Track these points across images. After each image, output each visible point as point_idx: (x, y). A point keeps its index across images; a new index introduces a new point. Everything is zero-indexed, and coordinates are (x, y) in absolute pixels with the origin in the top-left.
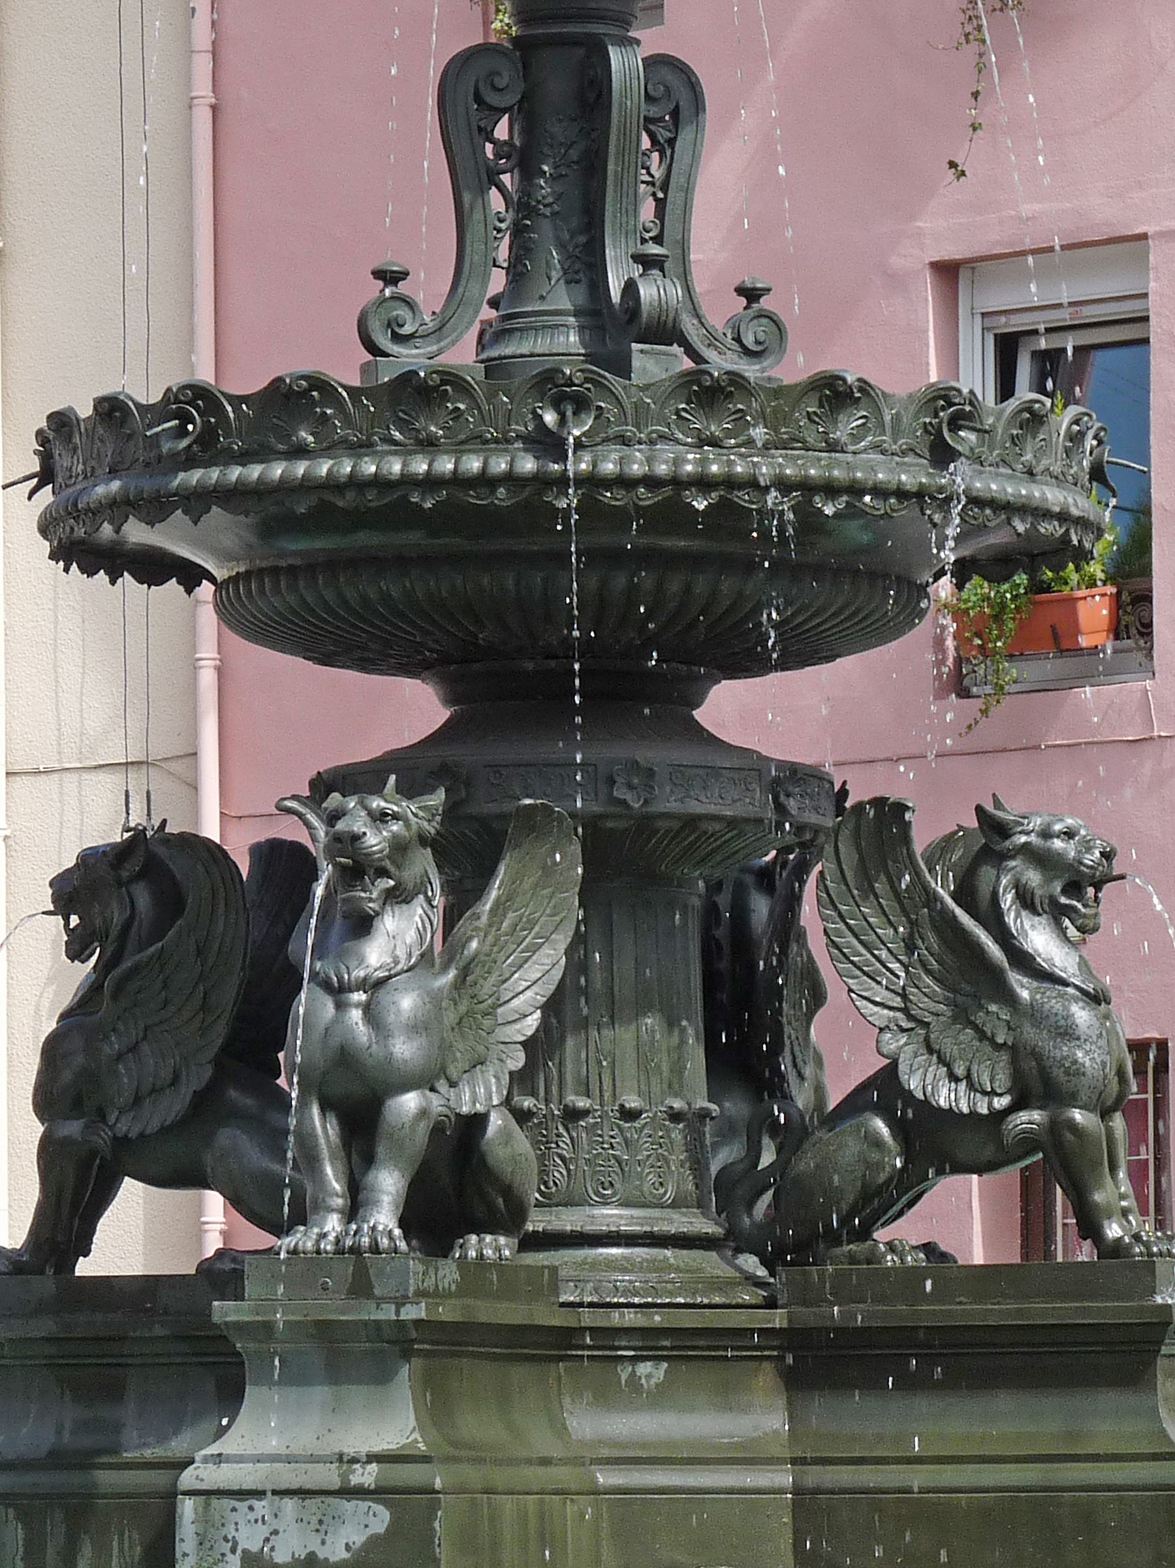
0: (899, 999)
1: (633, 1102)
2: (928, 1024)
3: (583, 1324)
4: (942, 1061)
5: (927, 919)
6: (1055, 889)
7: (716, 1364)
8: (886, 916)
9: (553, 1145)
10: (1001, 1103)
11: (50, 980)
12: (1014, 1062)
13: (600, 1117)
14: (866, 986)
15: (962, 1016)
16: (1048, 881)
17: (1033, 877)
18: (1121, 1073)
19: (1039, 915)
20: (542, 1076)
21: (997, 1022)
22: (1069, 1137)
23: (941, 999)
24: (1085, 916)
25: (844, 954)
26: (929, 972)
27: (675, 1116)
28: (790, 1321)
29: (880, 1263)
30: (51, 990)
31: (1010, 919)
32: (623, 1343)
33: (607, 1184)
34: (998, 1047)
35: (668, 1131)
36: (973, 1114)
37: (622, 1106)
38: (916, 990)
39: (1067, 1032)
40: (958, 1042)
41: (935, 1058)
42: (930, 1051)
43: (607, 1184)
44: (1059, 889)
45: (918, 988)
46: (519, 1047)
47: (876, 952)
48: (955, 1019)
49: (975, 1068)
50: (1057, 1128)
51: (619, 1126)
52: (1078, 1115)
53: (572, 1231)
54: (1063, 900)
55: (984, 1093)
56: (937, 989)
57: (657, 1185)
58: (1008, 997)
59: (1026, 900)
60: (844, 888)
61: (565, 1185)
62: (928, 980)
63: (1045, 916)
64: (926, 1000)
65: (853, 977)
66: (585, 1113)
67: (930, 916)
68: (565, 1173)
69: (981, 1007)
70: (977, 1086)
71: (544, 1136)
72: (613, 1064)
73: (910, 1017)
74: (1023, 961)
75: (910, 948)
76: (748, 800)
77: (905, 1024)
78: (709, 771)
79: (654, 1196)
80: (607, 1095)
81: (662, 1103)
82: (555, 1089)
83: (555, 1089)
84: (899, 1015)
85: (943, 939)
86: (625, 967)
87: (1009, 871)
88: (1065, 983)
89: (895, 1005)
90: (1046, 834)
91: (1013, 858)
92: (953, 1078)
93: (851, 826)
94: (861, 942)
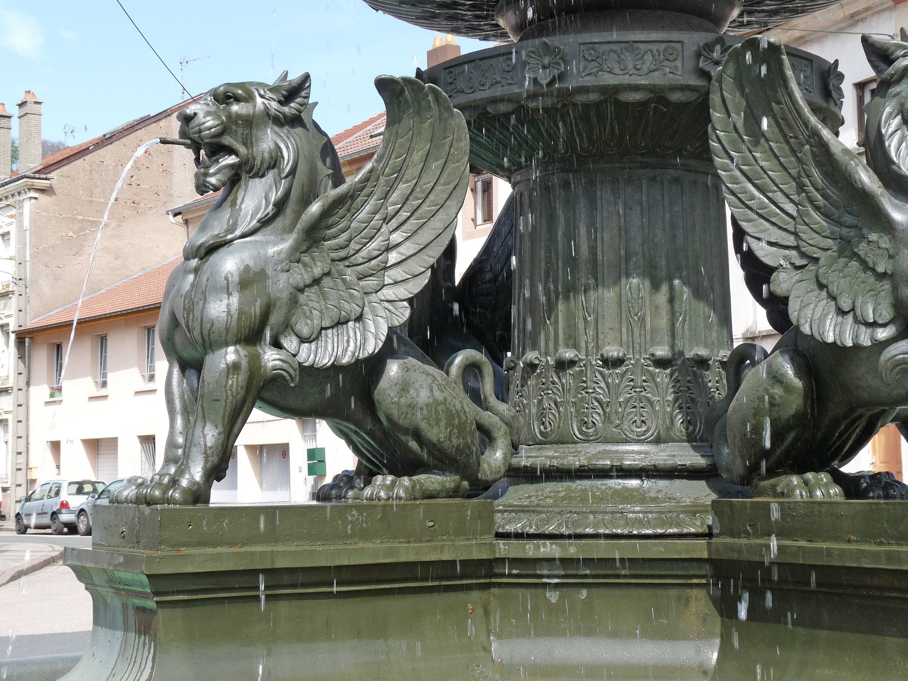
0: (792, 238)
1: (613, 351)
2: (817, 260)
3: (498, 556)
9: (550, 392)
10: (882, 334)
13: (584, 365)
20: (542, 336)
23: (827, 233)
26: (817, 208)
27: (661, 363)
28: (709, 551)
29: (789, 496)
32: (545, 572)
34: (882, 276)
35: (653, 376)
36: (857, 347)
40: (844, 278)
41: (824, 293)
43: (591, 424)
45: (806, 224)
46: (406, 304)
47: (770, 194)
48: (841, 253)
53: (524, 466)
55: (868, 325)
58: (886, 225)
60: (735, 135)
61: (556, 426)
62: (816, 216)
65: (749, 221)
66: (572, 363)
67: (812, 151)
68: (557, 416)
69: (863, 237)
70: (860, 318)
71: (543, 384)
72: (596, 319)
73: (803, 255)
76: (668, 70)
77: (799, 262)
81: (646, 351)
82: (551, 345)
83: (551, 345)
84: (794, 253)
85: (825, 174)
87: (895, 96)
89: (788, 244)
92: (841, 312)
93: (731, 70)
94: (755, 185)
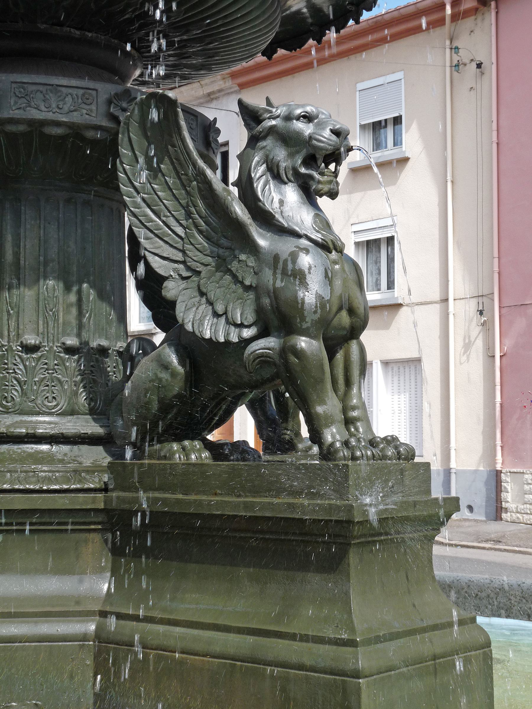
0: (180, 254)
1: (31, 340)
2: (199, 273)
4: (210, 303)
5: (196, 189)
6: (296, 161)
7: (52, 536)
8: (170, 189)
10: (247, 333)
11: (463, 348)
12: (258, 299)
14: (157, 245)
15: (222, 265)
16: (291, 155)
17: (280, 154)
18: (316, 307)
19: (285, 183)
21: (245, 269)
22: (293, 359)
23: (208, 252)
24: (319, 182)
25: (140, 221)
26: (200, 232)
27: (70, 350)
28: (105, 503)
30: (463, 349)
31: (259, 187)
33: (10, 399)
34: (248, 288)
36: (228, 343)
37: (22, 342)
38: (191, 247)
39: (300, 276)
40: (219, 287)
41: (204, 300)
42: (202, 294)
43: (10, 399)
44: (299, 162)
48: (218, 268)
49: (230, 309)
50: (289, 350)
51: (20, 357)
52: (303, 343)
54: (303, 170)
55: (237, 326)
56: (206, 245)
57: (50, 398)
58: (253, 248)
59: (275, 173)
62: (200, 238)
63: (290, 184)
64: (199, 254)
67: (198, 186)
70: (231, 320)
73: (188, 268)
74: (265, 219)
75: (189, 215)
77: (185, 274)
78: (49, 87)
79: (47, 407)
80: (13, 334)
81: (58, 340)
84: (181, 266)
85: (208, 206)
86: (29, 245)
88: (298, 236)
90: (288, 118)
91: (264, 138)
94: (153, 211)
